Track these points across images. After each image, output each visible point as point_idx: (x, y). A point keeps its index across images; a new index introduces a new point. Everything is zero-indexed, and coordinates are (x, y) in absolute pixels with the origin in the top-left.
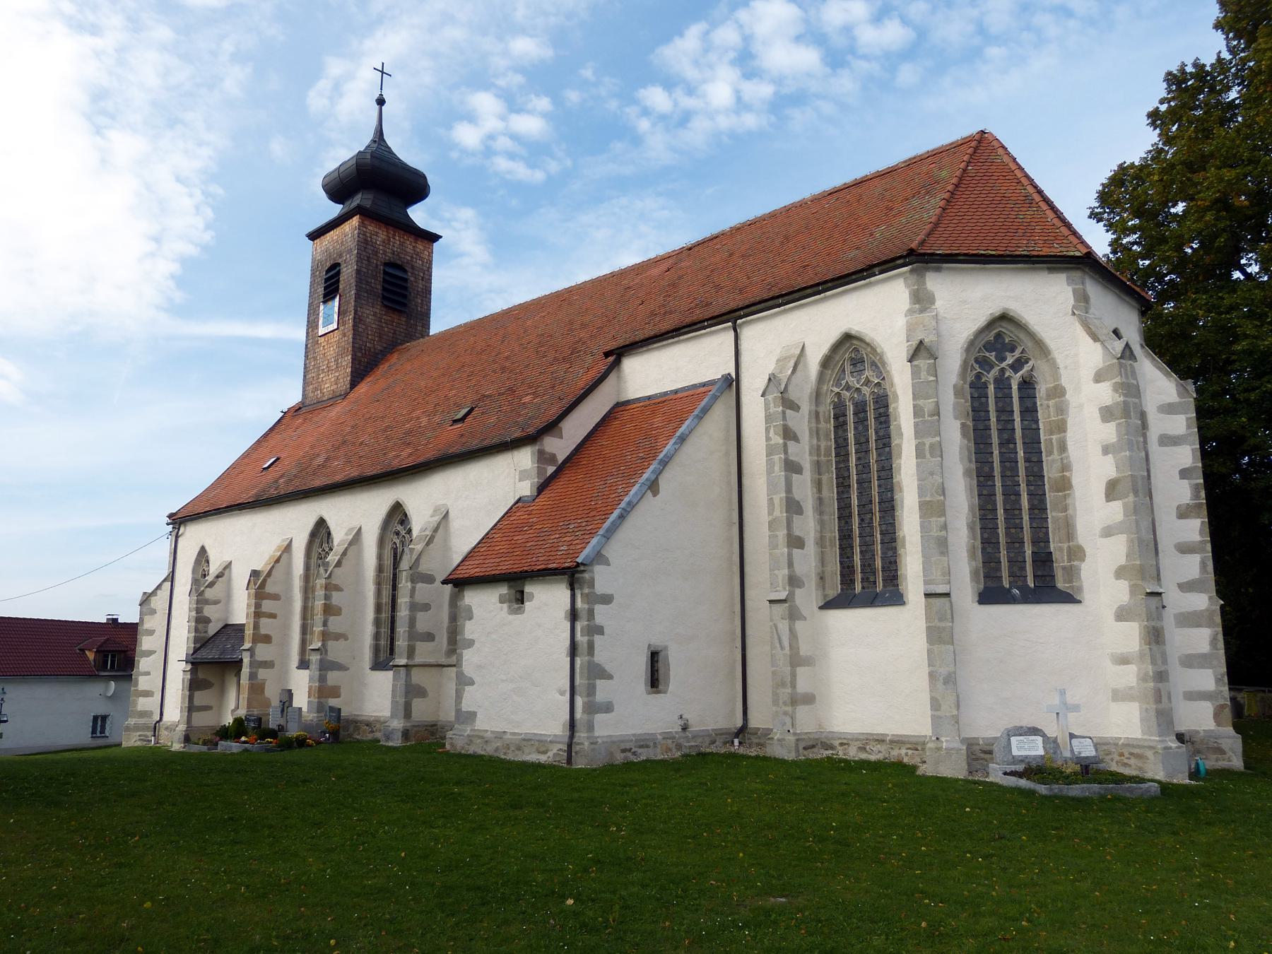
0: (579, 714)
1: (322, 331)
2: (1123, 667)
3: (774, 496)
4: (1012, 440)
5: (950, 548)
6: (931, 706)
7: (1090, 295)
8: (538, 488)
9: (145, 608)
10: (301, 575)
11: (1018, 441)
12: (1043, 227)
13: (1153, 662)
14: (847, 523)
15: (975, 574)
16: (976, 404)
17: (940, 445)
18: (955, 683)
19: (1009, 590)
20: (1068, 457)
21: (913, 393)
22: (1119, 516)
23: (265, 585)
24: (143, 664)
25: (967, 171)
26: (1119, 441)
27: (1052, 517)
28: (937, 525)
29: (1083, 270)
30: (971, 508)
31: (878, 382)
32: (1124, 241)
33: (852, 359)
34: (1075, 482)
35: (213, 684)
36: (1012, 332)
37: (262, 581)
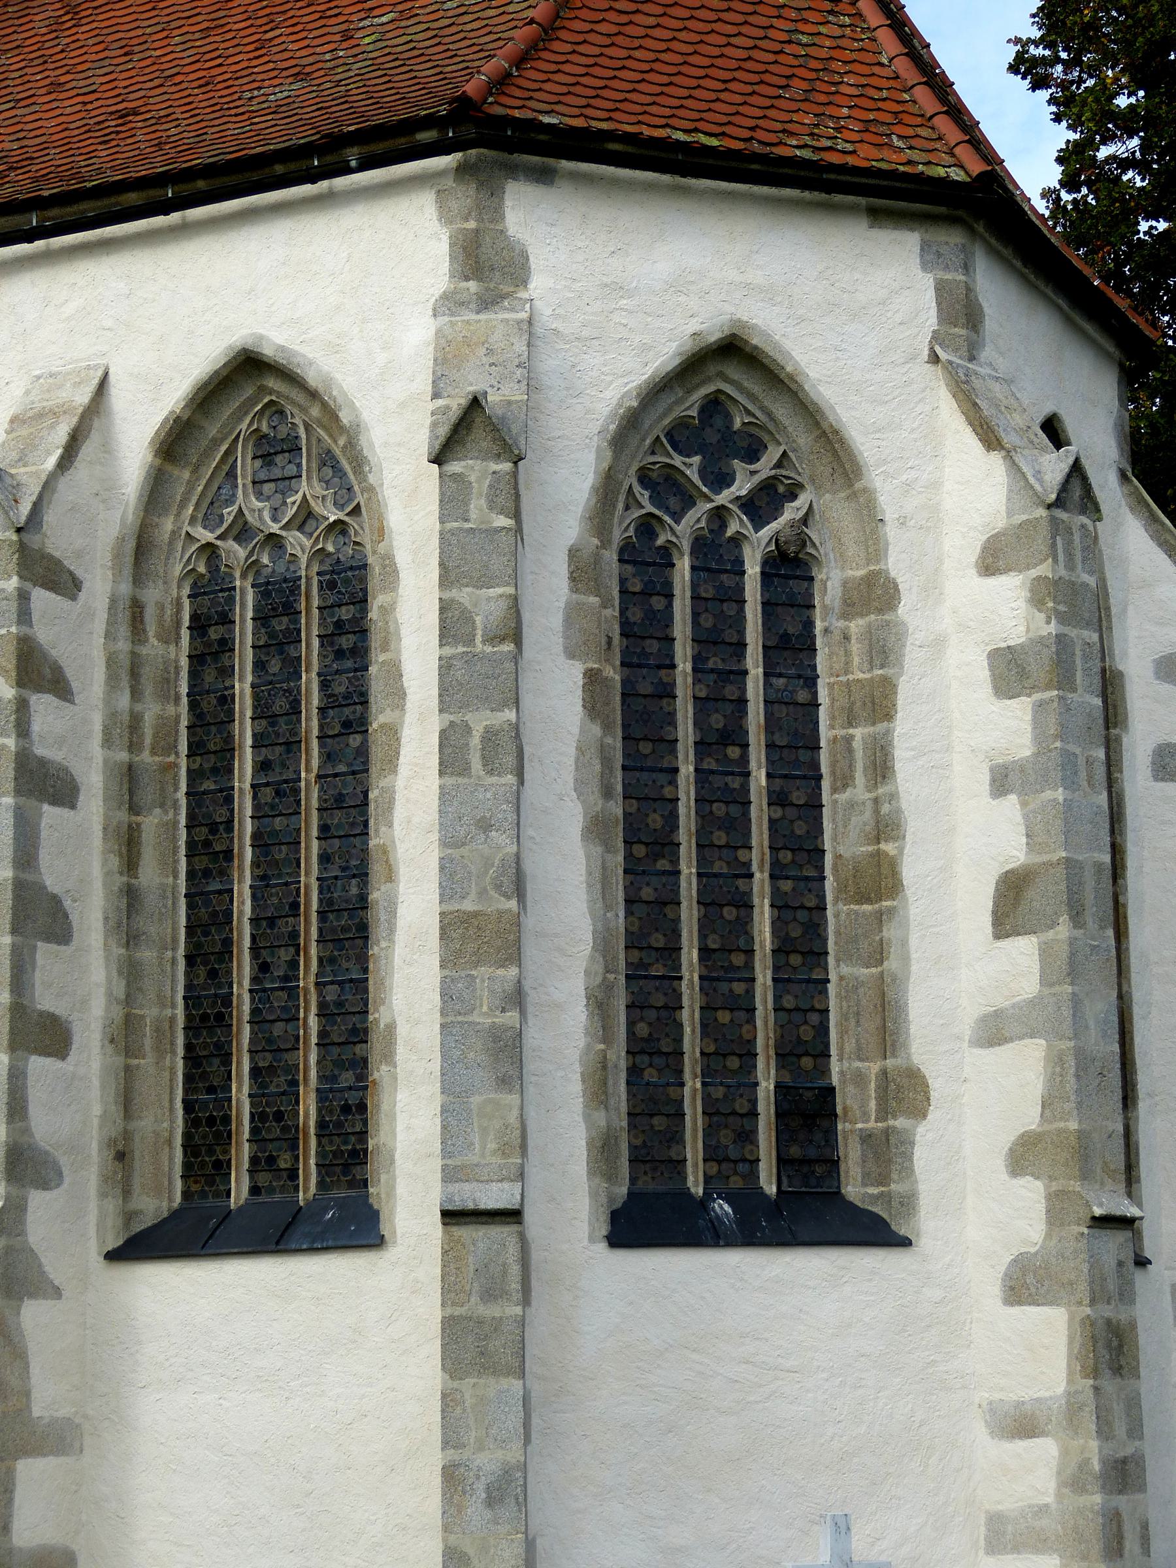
2: (1021, 1445)
4: (735, 735)
5: (530, 1066)
7: (985, 305)
11: (752, 739)
12: (864, 81)
13: (1104, 1431)
14: (213, 974)
16: (636, 615)
17: (518, 736)
18: (522, 1502)
19: (703, 1204)
20: (893, 797)
21: (442, 565)
22: (1029, 985)
26: (1037, 755)
27: (841, 978)
28: (492, 991)
29: (972, 232)
30: (603, 944)
31: (338, 522)
32: (1104, 152)
33: (260, 438)
34: (910, 872)
36: (752, 397)
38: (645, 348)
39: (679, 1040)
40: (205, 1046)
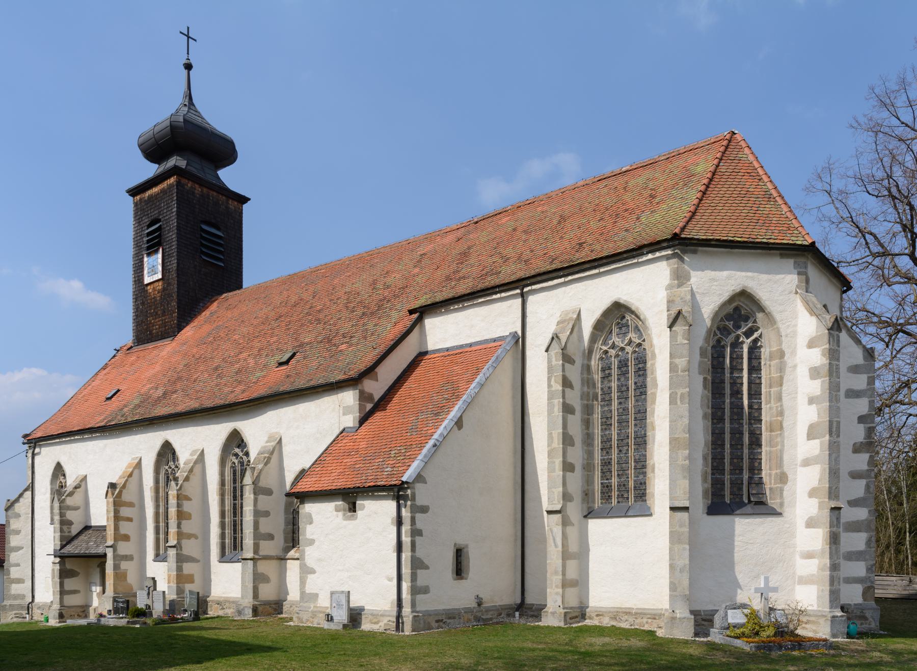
0: (406, 595)
1: (147, 280)
3: (553, 432)
6: (670, 588)
8: (359, 421)
9: (10, 512)
10: (151, 487)
12: (778, 219)
15: (705, 493)
16: (715, 363)
23: (121, 495)
24: (13, 557)
25: (719, 167)
30: (706, 444)
35: (79, 573)
37: (119, 492)
38: (720, 295)
39: (724, 467)
40: (606, 469)
